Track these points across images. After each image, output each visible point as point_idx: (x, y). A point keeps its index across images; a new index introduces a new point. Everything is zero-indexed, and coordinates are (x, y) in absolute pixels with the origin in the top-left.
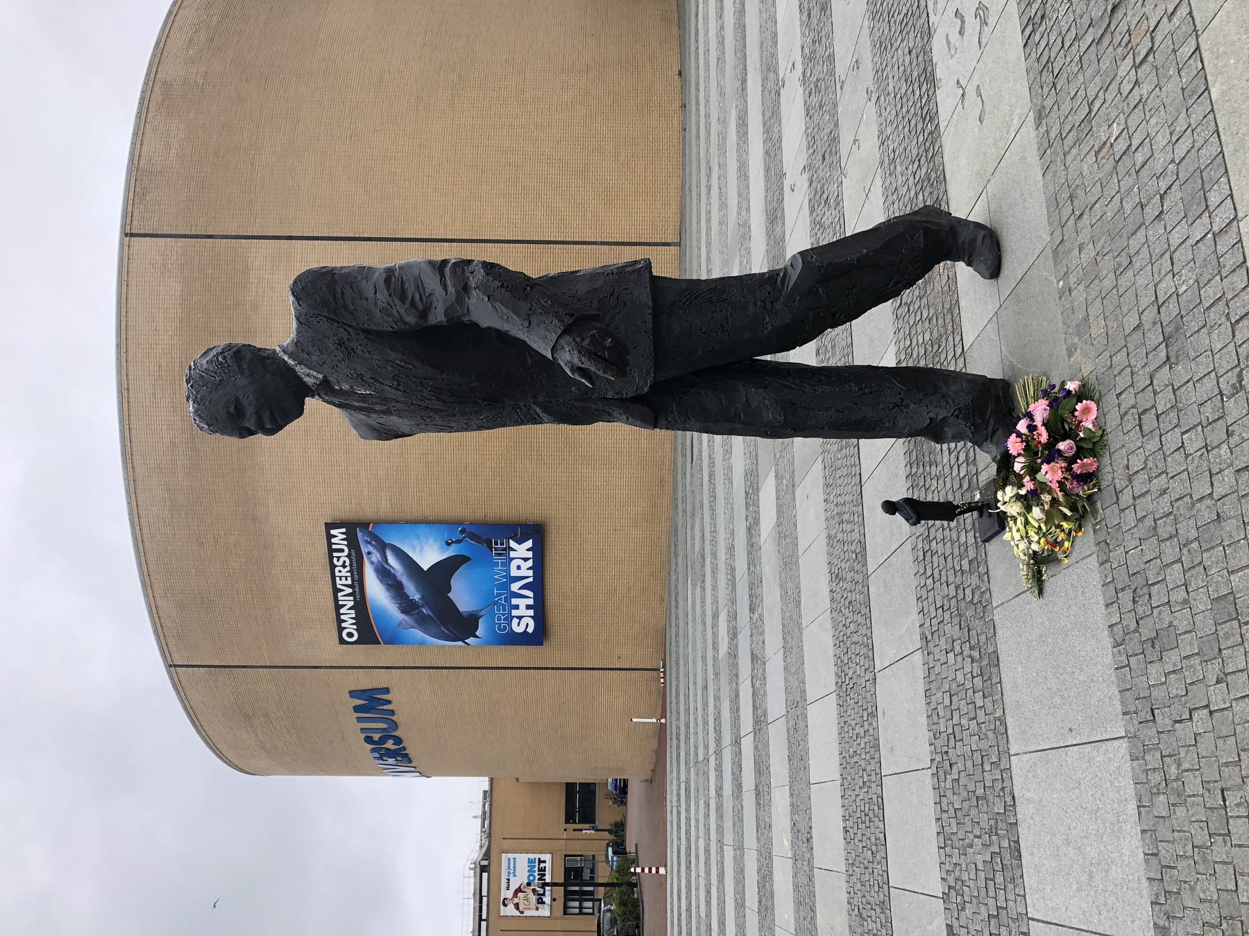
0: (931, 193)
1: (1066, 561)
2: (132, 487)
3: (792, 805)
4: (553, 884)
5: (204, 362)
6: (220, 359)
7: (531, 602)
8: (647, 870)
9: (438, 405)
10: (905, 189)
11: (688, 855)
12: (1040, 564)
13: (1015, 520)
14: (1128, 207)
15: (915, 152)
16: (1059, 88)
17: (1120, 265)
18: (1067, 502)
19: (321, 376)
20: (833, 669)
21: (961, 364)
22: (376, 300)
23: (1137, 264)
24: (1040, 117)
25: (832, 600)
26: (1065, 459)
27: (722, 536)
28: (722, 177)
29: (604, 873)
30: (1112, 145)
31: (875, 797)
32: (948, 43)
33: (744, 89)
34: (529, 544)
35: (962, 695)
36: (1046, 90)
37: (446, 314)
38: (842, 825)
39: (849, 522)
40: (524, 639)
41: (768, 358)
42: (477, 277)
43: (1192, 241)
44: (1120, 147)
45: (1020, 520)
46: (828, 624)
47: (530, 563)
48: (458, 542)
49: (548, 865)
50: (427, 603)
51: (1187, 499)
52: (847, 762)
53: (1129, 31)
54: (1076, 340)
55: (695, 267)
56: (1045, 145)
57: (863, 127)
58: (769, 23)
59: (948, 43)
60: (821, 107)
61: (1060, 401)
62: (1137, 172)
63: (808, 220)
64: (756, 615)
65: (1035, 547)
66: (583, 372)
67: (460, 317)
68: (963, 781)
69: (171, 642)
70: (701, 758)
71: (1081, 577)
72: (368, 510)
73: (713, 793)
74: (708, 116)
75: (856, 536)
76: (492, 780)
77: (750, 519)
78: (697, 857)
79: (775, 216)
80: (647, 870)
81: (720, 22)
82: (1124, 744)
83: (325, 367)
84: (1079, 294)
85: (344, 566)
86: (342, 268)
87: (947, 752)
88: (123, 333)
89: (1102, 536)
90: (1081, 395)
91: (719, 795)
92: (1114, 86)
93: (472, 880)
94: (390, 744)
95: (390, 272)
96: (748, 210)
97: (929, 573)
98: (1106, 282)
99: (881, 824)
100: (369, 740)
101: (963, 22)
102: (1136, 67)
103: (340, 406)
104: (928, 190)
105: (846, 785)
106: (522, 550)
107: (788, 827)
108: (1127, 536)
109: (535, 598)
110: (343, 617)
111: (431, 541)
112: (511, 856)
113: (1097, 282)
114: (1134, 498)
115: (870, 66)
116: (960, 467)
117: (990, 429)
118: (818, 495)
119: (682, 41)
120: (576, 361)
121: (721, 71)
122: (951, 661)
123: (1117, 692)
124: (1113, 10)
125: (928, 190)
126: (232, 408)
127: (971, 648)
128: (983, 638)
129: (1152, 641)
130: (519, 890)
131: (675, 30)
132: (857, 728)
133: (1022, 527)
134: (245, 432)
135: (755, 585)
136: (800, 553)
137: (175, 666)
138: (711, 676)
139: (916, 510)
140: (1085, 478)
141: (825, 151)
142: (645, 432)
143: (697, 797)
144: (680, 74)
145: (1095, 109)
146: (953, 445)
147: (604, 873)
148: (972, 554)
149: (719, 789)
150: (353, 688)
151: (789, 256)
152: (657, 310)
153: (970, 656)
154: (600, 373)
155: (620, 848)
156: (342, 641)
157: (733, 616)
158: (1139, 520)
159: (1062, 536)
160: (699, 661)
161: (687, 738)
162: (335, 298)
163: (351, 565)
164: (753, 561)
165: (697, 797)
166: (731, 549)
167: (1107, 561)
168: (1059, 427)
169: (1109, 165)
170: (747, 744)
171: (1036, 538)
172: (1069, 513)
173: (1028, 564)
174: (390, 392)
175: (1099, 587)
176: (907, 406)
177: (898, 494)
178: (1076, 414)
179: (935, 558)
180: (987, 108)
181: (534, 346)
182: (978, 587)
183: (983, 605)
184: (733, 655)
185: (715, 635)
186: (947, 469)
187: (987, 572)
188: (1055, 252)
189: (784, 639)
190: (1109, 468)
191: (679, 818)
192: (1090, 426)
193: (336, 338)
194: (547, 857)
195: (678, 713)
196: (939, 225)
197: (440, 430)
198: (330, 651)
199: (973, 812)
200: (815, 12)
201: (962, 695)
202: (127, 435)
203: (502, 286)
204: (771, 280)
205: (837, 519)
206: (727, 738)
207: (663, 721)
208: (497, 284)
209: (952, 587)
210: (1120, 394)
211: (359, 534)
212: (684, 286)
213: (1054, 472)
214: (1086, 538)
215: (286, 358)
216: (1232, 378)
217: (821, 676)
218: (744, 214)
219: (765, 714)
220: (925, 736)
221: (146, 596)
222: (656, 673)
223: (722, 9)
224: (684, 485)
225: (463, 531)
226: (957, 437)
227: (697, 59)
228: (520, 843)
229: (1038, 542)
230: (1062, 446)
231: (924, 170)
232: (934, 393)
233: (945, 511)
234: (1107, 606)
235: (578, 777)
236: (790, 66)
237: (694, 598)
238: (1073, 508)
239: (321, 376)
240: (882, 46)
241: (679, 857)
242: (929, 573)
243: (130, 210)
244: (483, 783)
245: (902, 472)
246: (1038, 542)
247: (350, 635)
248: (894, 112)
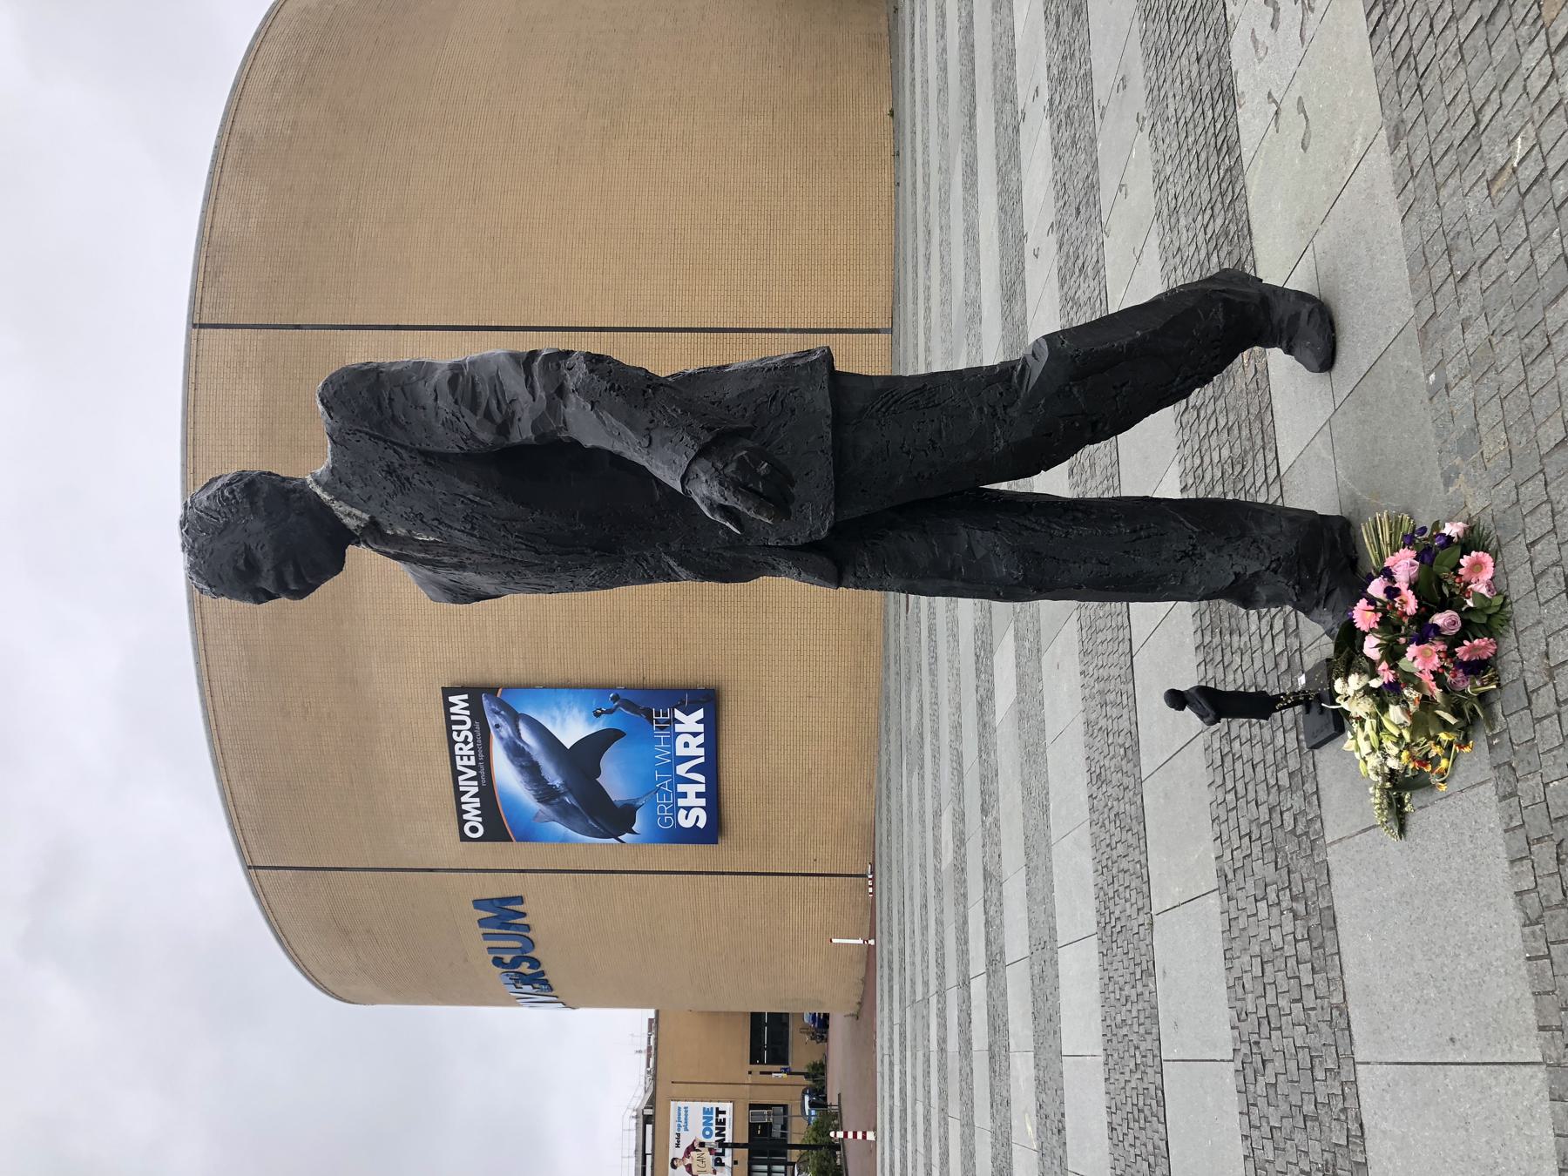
0: (1230, 253)
1: (1444, 788)
2: (201, 642)
3: (1037, 1079)
4: (734, 1146)
5: (204, 498)
6: (226, 493)
7: (702, 788)
8: (850, 1135)
9: (530, 557)
10: (1193, 247)
11: (903, 1120)
13: (1361, 721)
14: (1543, 262)
15: (1205, 197)
16: (1426, 91)
17: (1531, 350)
18: (1447, 702)
19: (366, 516)
20: (1094, 904)
21: (1275, 492)
22: (437, 408)
24: (1397, 135)
25: (1092, 809)
26: (1445, 639)
27: (945, 710)
28: (945, 243)
29: (799, 1132)
30: (1514, 171)
31: (1152, 1087)
32: (1255, 41)
33: (972, 127)
34: (700, 714)
35: (1280, 963)
36: (1406, 96)
37: (534, 428)
38: (1105, 1118)
39: (1114, 704)
41: (1003, 486)
42: (577, 375)
44: (1529, 172)
45: (1370, 724)
46: (1087, 841)
47: (701, 739)
48: (609, 712)
49: (728, 1117)
50: (570, 790)
52: (1111, 1032)
53: (1442, 83)
54: (1458, 461)
55: (911, 360)
56: (1406, 177)
57: (1131, 167)
58: (1005, 39)
59: (1255, 41)
60: (1074, 143)
61: (1436, 553)
62: (1557, 210)
63: (1057, 295)
64: (990, 819)
65: (1393, 763)
66: (727, 512)
67: (554, 432)
68: (1283, 1088)
70: (919, 997)
71: (1469, 807)
72: (495, 672)
73: (934, 1046)
74: (926, 164)
75: (1124, 724)
76: (657, 1013)
77: (981, 690)
78: (914, 1125)
79: (1012, 291)
80: (850, 1135)
81: (941, 43)
82: (1541, 1074)
83: (371, 503)
84: (1463, 393)
85: (466, 742)
86: (392, 364)
87: (1257, 1043)
88: (190, 448)
89: (1504, 755)
90: (1468, 543)
91: (942, 1050)
92: (1516, 84)
93: (633, 1134)
94: (525, 968)
95: (457, 369)
96: (978, 284)
97: (1230, 785)
98: (1507, 375)
99: (1161, 1128)
100: (498, 962)
101: (1277, 10)
103: (396, 557)
104: (1225, 249)
105: (1111, 1067)
106: (690, 722)
107: (1033, 1108)
108: (1548, 760)
110: (464, 807)
111: (575, 711)
112: (682, 1104)
113: (1492, 374)
114: (1558, 703)
116: (1279, 642)
117: (1323, 588)
118: (1073, 665)
119: (895, 71)
120: (716, 496)
121: (943, 105)
122: (1263, 913)
123: (1529, 995)
125: (1225, 249)
127: (1293, 898)
128: (1311, 886)
130: (691, 1148)
131: (885, 56)
132: (1127, 987)
133: (1372, 734)
134: (260, 596)
135: (988, 778)
136: (1048, 741)
138: (932, 892)
139: (1214, 703)
140: (1476, 668)
141: (1080, 200)
142: (832, 591)
143: (914, 1047)
144: (892, 114)
145: (1486, 119)
146: (1264, 610)
147: (799, 1132)
148: (1293, 763)
149: (942, 1041)
150: (478, 897)
151: (1031, 340)
152: (839, 420)
153: (1291, 910)
154: (751, 514)
155: (819, 1100)
156: (464, 838)
157: (960, 817)
159: (1435, 751)
161: (902, 969)
162: (380, 407)
163: (475, 740)
165: (914, 1047)
166: (957, 728)
167: (1513, 794)
168: (1436, 590)
170: (978, 987)
171: (1394, 750)
172: (1452, 721)
173: (1382, 789)
174: (462, 539)
175: (1500, 831)
176: (1202, 556)
177: (1186, 683)
178: (1461, 571)
179: (1238, 765)
180: (1313, 128)
181: (658, 474)
182: (1304, 813)
183: (1310, 836)
184: (960, 868)
185: (937, 840)
186: (1256, 640)
187: (1317, 792)
188: (1423, 332)
189: (1027, 854)
190: (1515, 655)
191: (892, 1071)
192: (1484, 591)
193: (383, 463)
194: (727, 1107)
195: (891, 935)
196: (1246, 295)
197: (537, 591)
198: (450, 850)
199: (1299, 1136)
200: (1067, 18)
201: (1280, 963)
203: (612, 388)
204: (1004, 375)
205: (1098, 698)
206: (952, 978)
207: (872, 942)
208: (605, 384)
209: (1264, 809)
210: (1533, 543)
211: (485, 703)
212: (878, 386)
213: (1427, 659)
214: (1476, 758)
215: (319, 491)
217: (1077, 912)
218: (972, 289)
219: (1002, 953)
220: (1224, 1015)
221: (219, 780)
222: (863, 878)
223: (944, 27)
224: (897, 640)
225: (615, 698)
226: (1276, 600)
228: (693, 1088)
229: (1398, 757)
230: (1439, 619)
231: (1219, 221)
232: (1241, 536)
233: (1257, 705)
234: (1512, 862)
235: (766, 1008)
236: (1032, 92)
237: (910, 787)
238: (1457, 712)
239: (366, 516)
240: (1158, 55)
241: (891, 1121)
242: (1230, 785)
243: (199, 295)
244: (651, 1013)
245: (1191, 641)
246: (1398, 757)
248: (1175, 144)
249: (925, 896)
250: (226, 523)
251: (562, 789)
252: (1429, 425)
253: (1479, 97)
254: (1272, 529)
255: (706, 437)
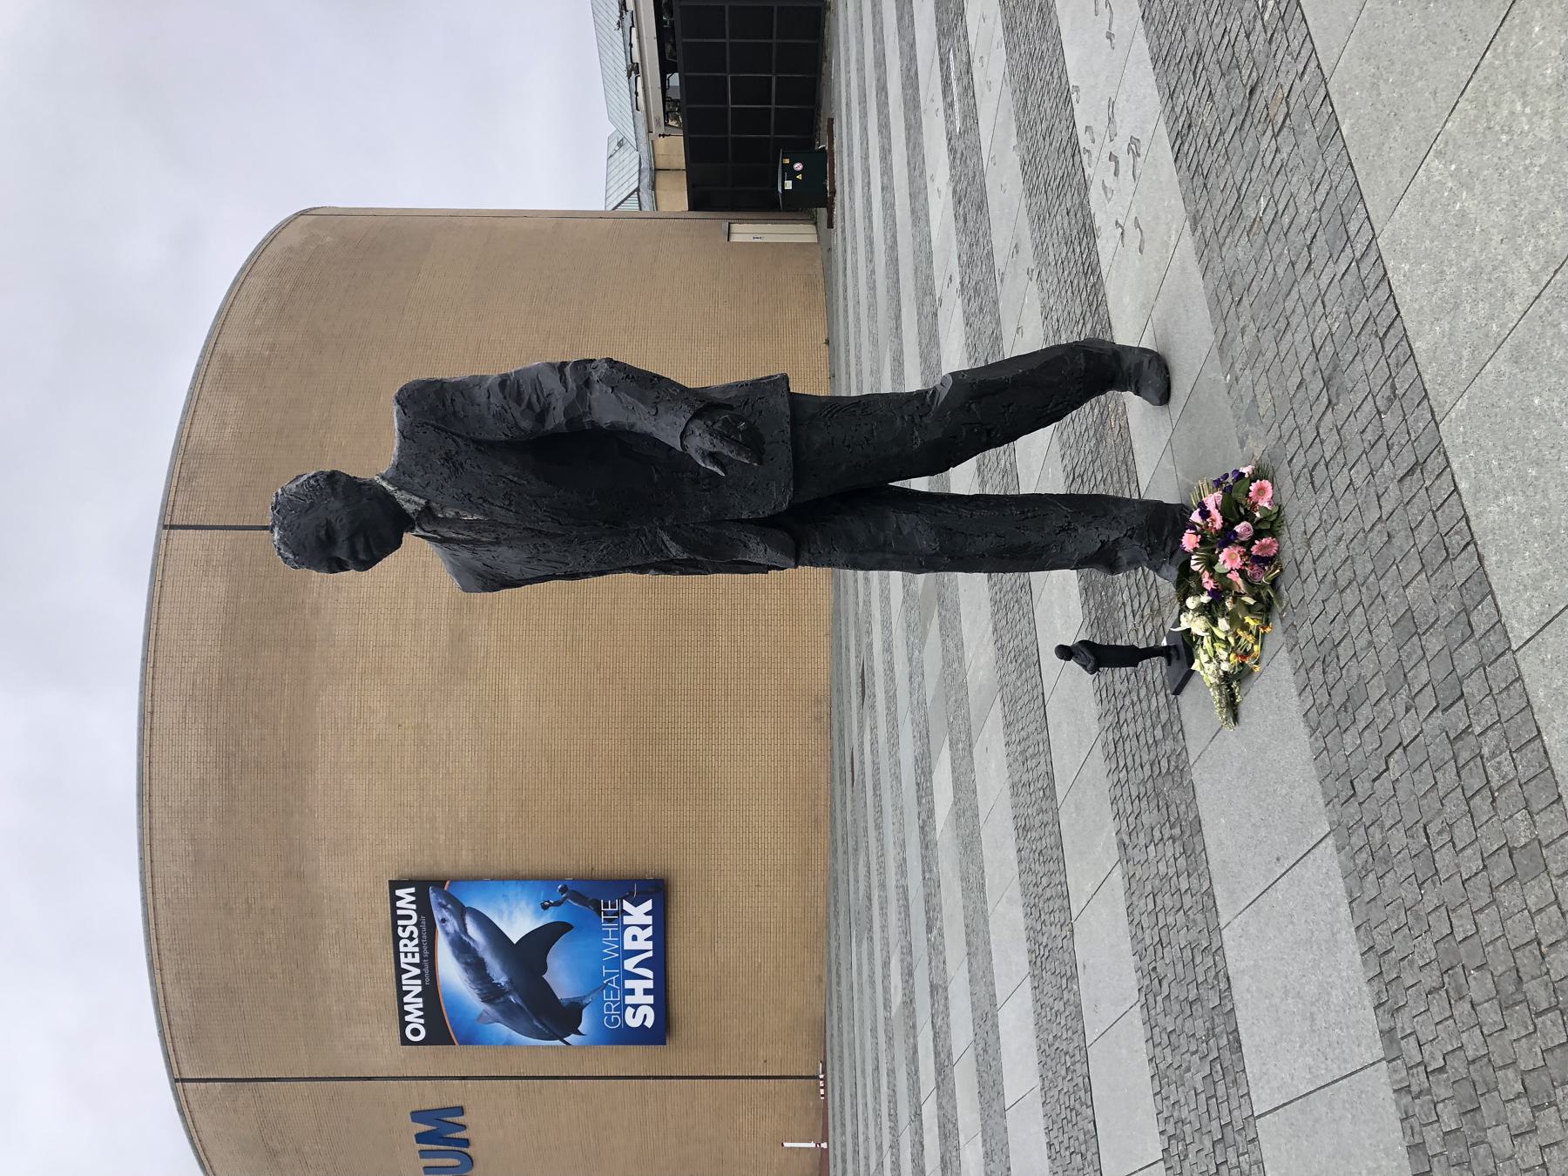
2: (147, 838)
7: (650, 984)
12: (1232, 683)
14: (1280, 272)
19: (423, 502)
22: (489, 404)
23: (1294, 321)
24: (1195, 221)
26: (1242, 544)
33: (898, 327)
38: (1044, 1140)
40: (641, 1036)
43: (1338, 277)
44: (1268, 218)
47: (649, 932)
48: (558, 904)
51: (1361, 535)
65: (1225, 667)
69: (180, 1045)
83: (429, 489)
84: (1246, 380)
85: (411, 938)
88: (152, 644)
92: (1259, 162)
95: (504, 381)
97: (1122, 764)
101: (1117, 163)
102: (1275, 136)
106: (638, 914)
109: (655, 979)
110: (407, 1008)
115: (1029, 246)
116: (1142, 602)
117: (1168, 550)
121: (873, 317)
124: (1251, 93)
126: (323, 533)
129: (1344, 706)
137: (183, 1080)
139: (1095, 655)
144: (827, 342)
148: (1164, 717)
150: (417, 1108)
152: (795, 421)
156: (405, 1041)
158: (1321, 582)
160: (866, 987)
163: (420, 937)
164: (928, 864)
168: (1234, 509)
169: (1260, 240)
174: (501, 514)
187: (1181, 729)
188: (1220, 349)
195: (843, 1125)
200: (972, 215)
202: (146, 770)
207: (824, 1145)
208: (622, 375)
211: (432, 896)
215: (384, 484)
216: (1387, 391)
225: (564, 890)
226: (1134, 563)
227: (846, 317)
231: (1089, 326)
233: (1129, 656)
238: (1257, 597)
239: (423, 502)
240: (1040, 220)
242: (1122, 764)
247: (415, 1032)
249: (877, 1059)
250: (312, 505)
251: (507, 988)
252: (1230, 411)
253: (1238, 179)
254: (1126, 510)
255: (699, 405)
